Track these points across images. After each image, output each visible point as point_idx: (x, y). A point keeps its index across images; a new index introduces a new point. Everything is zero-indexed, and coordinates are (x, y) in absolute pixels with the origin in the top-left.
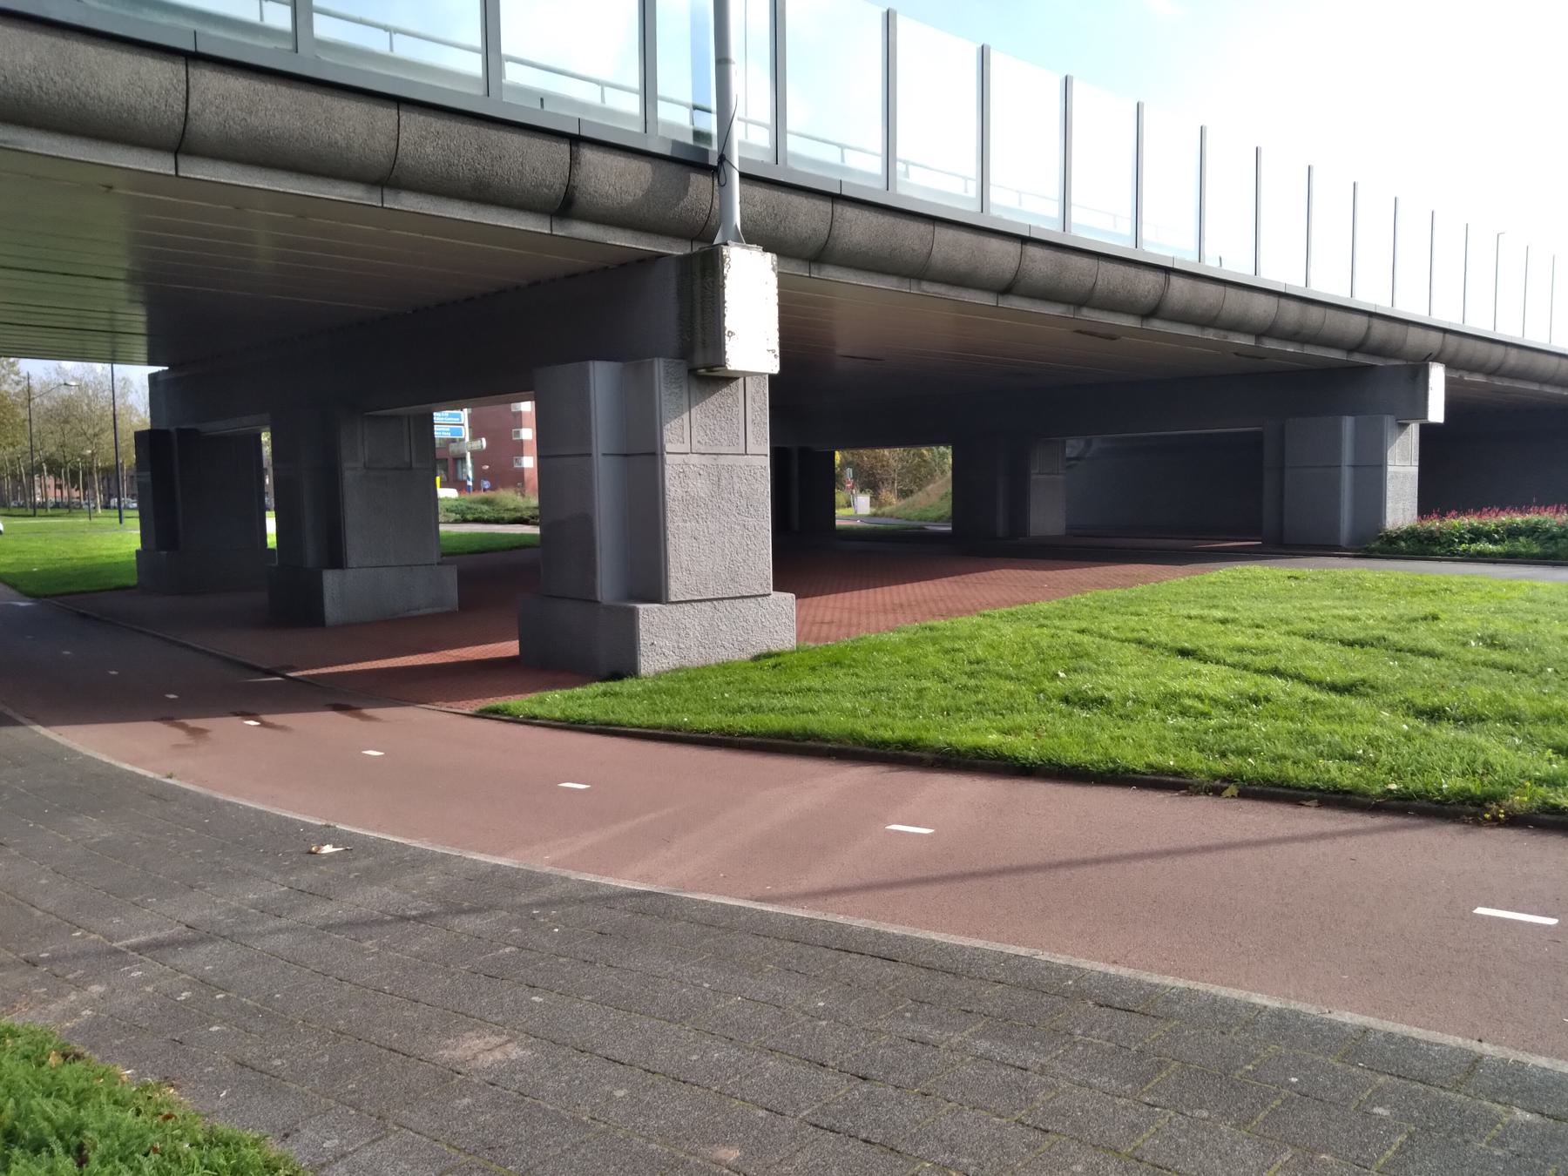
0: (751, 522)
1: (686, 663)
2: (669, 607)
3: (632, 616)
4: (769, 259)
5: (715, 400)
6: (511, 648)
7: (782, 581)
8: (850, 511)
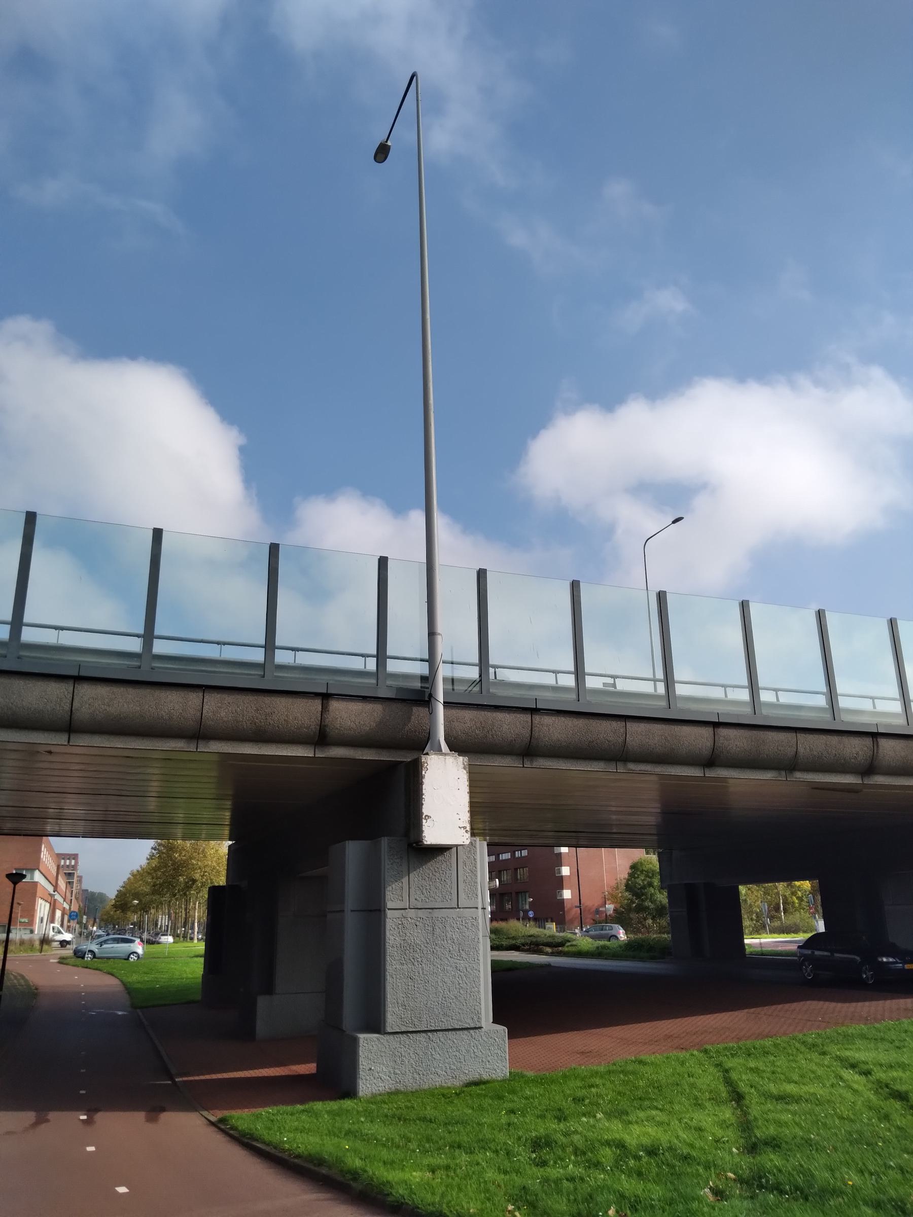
1: (401, 1087)
2: (387, 1037)
3: (355, 1041)
4: (461, 760)
5: (432, 865)
6: (310, 1068)
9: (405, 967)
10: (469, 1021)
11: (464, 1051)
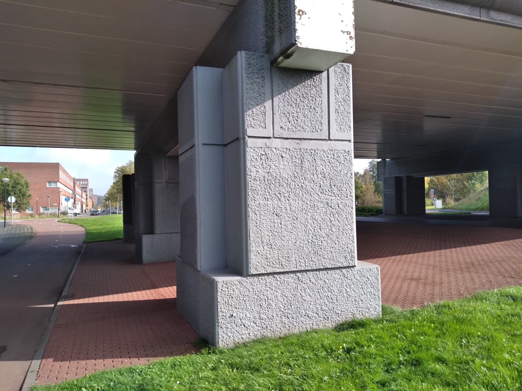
0: (335, 201)
2: (250, 279)
5: (297, 91)
7: (365, 252)
8: (433, 207)
9: (270, 202)
10: (342, 260)
11: (336, 290)
